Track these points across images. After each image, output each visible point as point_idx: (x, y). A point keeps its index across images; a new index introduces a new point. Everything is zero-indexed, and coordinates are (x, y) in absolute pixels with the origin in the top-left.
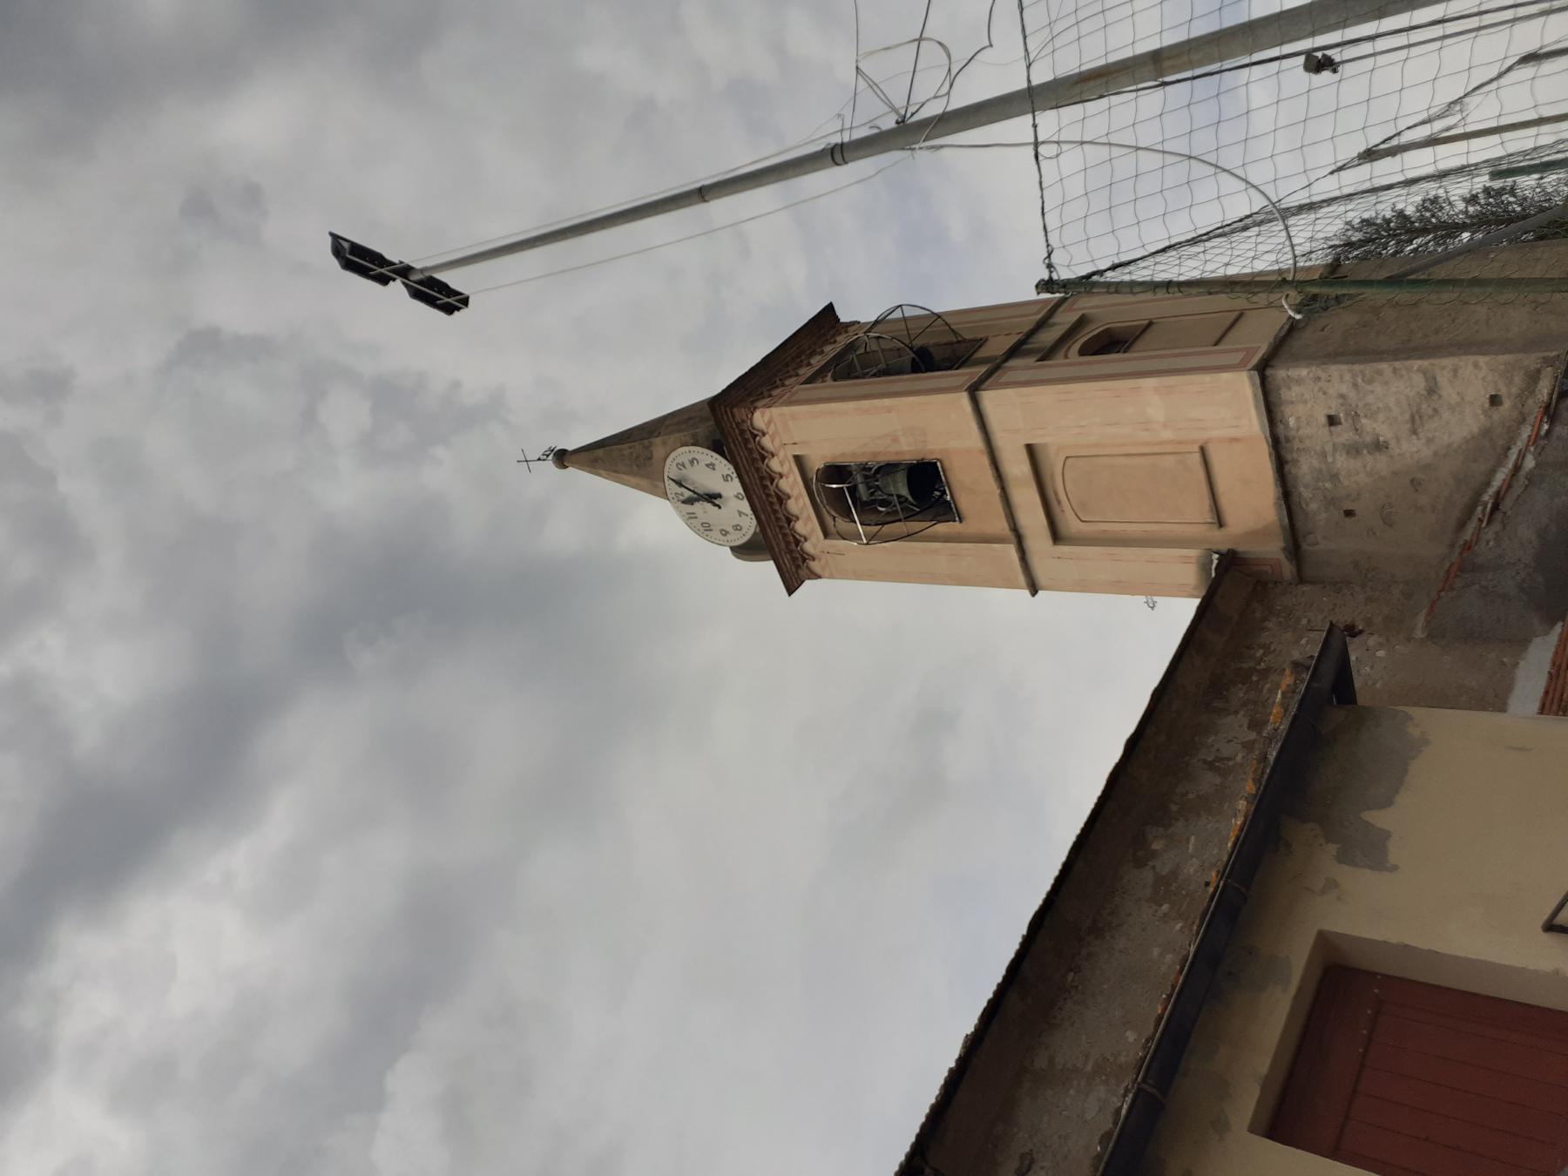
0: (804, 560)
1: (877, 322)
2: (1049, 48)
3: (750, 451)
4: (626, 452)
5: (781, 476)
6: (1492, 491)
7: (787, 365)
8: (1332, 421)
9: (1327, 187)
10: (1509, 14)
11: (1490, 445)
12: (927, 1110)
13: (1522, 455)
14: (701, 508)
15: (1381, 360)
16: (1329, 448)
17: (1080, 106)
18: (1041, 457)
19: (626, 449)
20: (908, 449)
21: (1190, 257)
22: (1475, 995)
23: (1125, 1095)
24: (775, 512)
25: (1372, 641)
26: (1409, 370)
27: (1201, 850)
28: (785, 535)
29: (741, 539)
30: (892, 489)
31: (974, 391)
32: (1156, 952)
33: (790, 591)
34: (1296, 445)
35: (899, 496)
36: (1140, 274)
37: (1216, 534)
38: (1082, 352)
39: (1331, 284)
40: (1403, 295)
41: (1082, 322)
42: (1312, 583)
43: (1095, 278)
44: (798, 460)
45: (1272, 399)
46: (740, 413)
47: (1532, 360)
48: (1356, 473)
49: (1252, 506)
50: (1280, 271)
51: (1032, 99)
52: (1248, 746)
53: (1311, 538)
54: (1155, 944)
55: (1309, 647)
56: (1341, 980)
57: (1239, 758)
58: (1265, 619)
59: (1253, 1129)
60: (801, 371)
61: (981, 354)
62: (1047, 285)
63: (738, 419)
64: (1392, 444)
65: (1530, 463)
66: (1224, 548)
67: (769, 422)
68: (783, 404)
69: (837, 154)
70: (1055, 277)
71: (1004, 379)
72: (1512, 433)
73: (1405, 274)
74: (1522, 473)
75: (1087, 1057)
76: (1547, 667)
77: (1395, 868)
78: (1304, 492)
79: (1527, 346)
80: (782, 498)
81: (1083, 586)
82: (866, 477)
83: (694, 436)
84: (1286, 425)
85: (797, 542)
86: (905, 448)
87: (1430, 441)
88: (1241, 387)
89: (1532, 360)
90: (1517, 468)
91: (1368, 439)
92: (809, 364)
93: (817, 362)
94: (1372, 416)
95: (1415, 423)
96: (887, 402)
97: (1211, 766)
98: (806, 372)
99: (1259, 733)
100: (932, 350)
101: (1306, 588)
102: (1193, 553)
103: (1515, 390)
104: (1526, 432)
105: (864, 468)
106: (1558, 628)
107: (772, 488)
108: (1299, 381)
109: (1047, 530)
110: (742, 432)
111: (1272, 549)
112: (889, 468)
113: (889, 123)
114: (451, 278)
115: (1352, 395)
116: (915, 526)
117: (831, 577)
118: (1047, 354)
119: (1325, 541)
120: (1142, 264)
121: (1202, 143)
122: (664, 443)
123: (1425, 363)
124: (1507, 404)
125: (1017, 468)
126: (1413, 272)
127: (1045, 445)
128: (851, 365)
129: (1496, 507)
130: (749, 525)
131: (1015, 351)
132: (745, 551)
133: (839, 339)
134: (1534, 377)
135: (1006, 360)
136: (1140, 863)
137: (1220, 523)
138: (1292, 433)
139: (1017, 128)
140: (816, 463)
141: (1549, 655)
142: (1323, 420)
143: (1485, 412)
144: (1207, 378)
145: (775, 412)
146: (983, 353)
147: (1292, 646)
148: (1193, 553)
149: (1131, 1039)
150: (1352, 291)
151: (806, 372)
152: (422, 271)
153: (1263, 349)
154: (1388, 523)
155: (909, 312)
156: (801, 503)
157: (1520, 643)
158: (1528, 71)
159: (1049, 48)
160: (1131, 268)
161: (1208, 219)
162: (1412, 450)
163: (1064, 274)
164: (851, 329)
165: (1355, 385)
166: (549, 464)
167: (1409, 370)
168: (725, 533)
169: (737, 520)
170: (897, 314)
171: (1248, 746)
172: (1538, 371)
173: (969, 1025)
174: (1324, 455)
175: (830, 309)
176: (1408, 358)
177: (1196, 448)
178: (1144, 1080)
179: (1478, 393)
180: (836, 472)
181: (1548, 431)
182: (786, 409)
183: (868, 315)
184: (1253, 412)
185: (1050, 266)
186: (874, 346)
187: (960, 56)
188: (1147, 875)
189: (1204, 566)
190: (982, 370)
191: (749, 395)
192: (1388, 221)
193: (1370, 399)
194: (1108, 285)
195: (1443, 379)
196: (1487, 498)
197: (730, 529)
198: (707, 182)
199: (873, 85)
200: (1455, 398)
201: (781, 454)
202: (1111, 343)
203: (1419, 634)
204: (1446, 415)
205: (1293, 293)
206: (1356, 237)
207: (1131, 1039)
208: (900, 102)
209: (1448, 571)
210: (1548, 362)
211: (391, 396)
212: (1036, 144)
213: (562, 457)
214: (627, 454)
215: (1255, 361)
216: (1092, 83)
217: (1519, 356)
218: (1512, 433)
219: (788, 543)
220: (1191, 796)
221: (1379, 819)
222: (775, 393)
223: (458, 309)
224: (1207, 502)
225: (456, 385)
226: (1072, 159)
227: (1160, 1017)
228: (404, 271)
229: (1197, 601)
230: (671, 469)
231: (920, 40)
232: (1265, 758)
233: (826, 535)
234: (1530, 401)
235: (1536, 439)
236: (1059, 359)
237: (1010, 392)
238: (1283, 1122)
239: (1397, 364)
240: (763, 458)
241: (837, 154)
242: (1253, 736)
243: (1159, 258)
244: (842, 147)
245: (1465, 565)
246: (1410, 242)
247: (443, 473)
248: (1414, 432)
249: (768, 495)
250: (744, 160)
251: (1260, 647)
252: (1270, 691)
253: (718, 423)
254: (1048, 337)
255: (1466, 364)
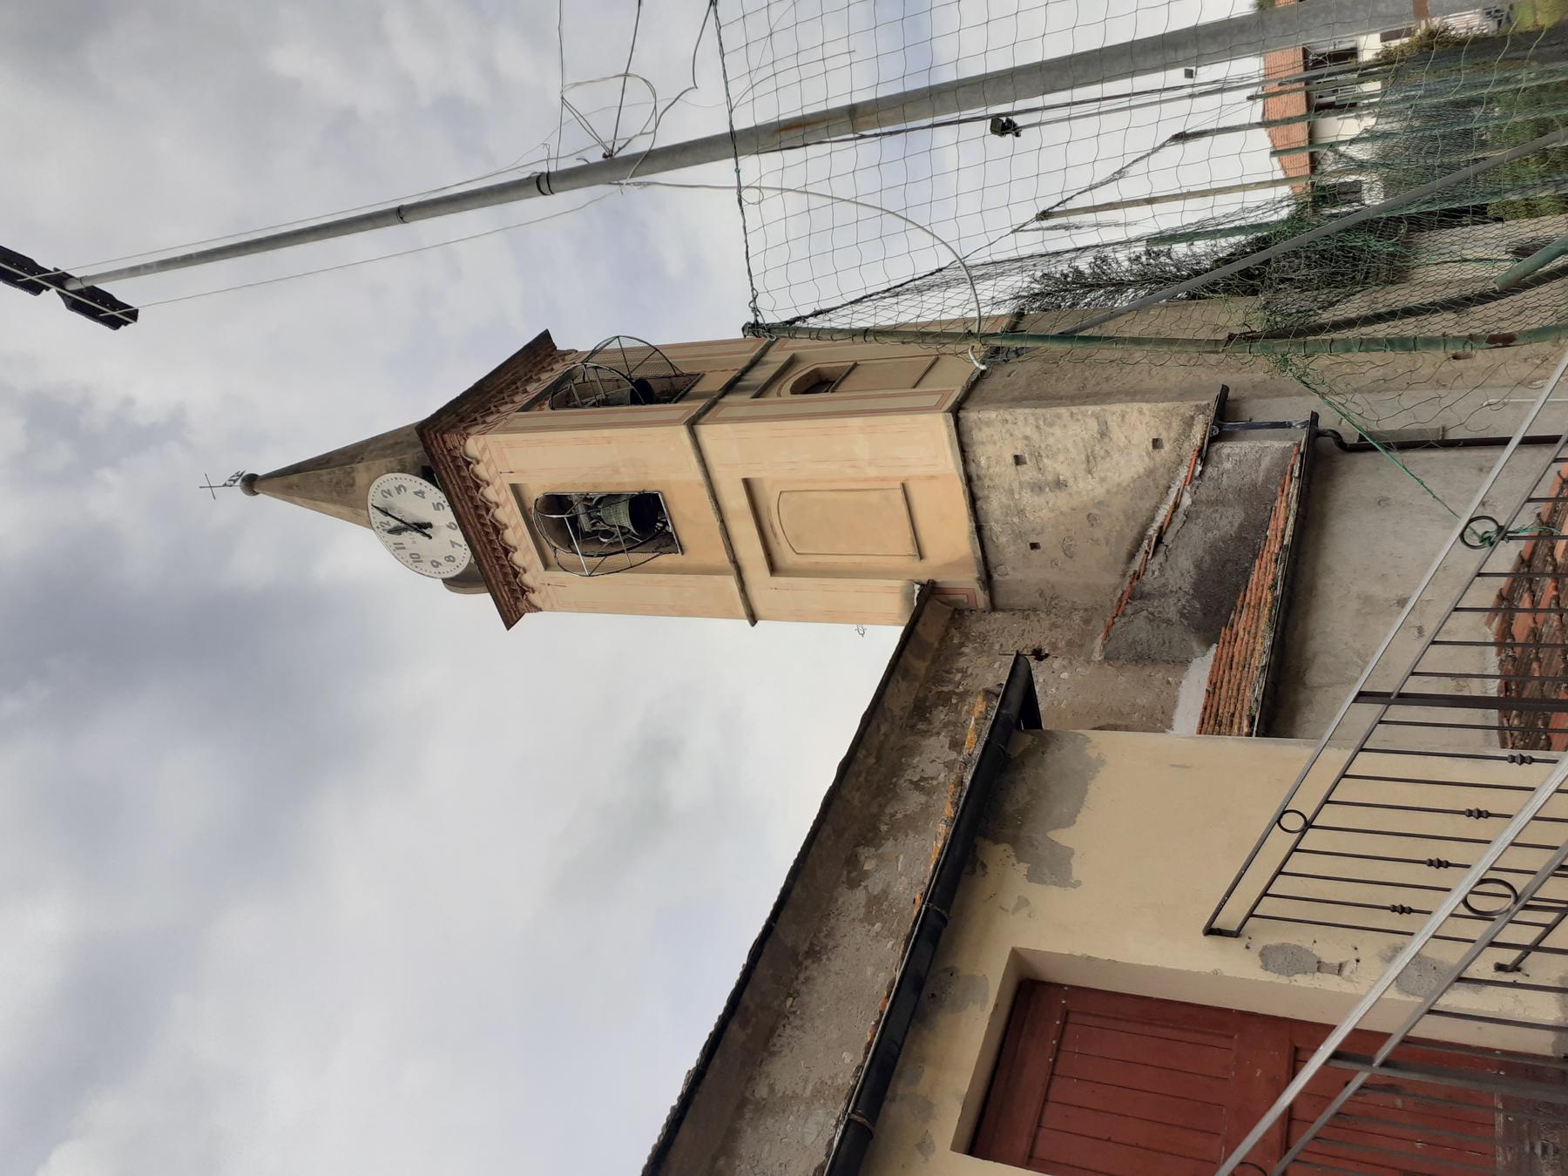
0: (524, 592)
1: (594, 352)
2: (749, 96)
3: (463, 479)
4: (325, 478)
5: (497, 506)
6: (1156, 526)
7: (501, 392)
8: (1018, 460)
9: (1008, 248)
10: (1156, 97)
11: (1154, 483)
12: (649, 1152)
13: (1180, 495)
14: (409, 537)
15: (1059, 405)
16: (1016, 485)
17: (778, 154)
18: (756, 489)
19: (325, 475)
20: (630, 481)
21: (885, 308)
22: (1150, 998)
23: (836, 1127)
24: (491, 542)
25: (1057, 664)
26: (1084, 414)
27: (906, 868)
28: (502, 566)
29: (454, 571)
30: (614, 521)
31: (692, 424)
32: (870, 971)
33: (509, 625)
34: (987, 482)
35: (621, 527)
36: (839, 321)
37: (918, 565)
38: (794, 391)
39: (1012, 338)
40: (1079, 349)
41: (792, 362)
42: (1003, 610)
43: (798, 323)
44: (515, 489)
45: (966, 439)
46: (452, 439)
47: (1186, 408)
48: (1041, 510)
49: (949, 546)
50: (965, 321)
51: (735, 143)
52: (949, 765)
53: (1001, 569)
54: (864, 964)
55: (996, 673)
56: (1032, 994)
57: (941, 778)
58: (962, 645)
59: (954, 1148)
60: (517, 398)
61: (698, 389)
62: (754, 328)
63: (449, 445)
64: (1071, 482)
65: (1187, 501)
66: (924, 579)
67: (484, 449)
68: (497, 431)
69: (543, 183)
70: (760, 320)
71: (722, 414)
72: (1172, 473)
73: (1076, 331)
74: (1181, 510)
75: (806, 1081)
76: (1205, 685)
77: (1078, 883)
78: (994, 527)
79: (1182, 395)
80: (498, 529)
81: (799, 616)
82: (588, 508)
83: (401, 462)
84: (978, 465)
85: (516, 574)
86: (626, 479)
87: (1103, 480)
88: (938, 427)
89: (1186, 408)
90: (1176, 506)
91: (1050, 478)
92: (525, 391)
93: (534, 389)
94: (1054, 456)
95: (1090, 462)
96: (606, 432)
97: (917, 785)
98: (522, 399)
99: (960, 753)
100: (647, 384)
101: (998, 615)
102: (898, 583)
103: (1173, 435)
104: (1183, 472)
105: (586, 498)
106: (1213, 650)
107: (488, 517)
108: (989, 424)
109: (765, 563)
110: (454, 459)
111: (965, 580)
112: (611, 499)
113: (596, 156)
114: (120, 290)
115: (1035, 436)
116: (636, 557)
117: (552, 609)
118: (761, 392)
119: (1015, 572)
120: (841, 312)
121: (893, 201)
122: (368, 469)
123: (1097, 408)
124: (1167, 447)
125: (735, 501)
126: (1082, 329)
127: (761, 480)
128: (569, 394)
129: (1159, 540)
130: (463, 557)
131: (730, 388)
132: (458, 583)
133: (556, 367)
134: (1189, 423)
135: (722, 396)
136: (853, 884)
137: (921, 556)
138: (983, 472)
139: (720, 170)
140: (536, 490)
141: (1207, 674)
142: (1011, 460)
143: (1148, 453)
144: (906, 419)
145: (490, 438)
146: (700, 388)
147: (987, 671)
148: (898, 583)
149: (847, 1060)
150: (1029, 344)
151: (522, 399)
152: (81, 280)
153: (957, 392)
154: (1069, 553)
155: (626, 344)
156: (519, 533)
157: (1182, 663)
158: (1177, 149)
159: (749, 96)
160: (830, 315)
161: (901, 272)
162: (1087, 488)
163: (768, 318)
164: (568, 358)
165: (1038, 427)
166: (237, 491)
167: (1084, 414)
168: (436, 564)
169: (450, 551)
170: (615, 345)
171: (949, 765)
172: (1192, 418)
173: (690, 1059)
174: (1012, 492)
175: (545, 337)
176: (1083, 404)
177: (898, 485)
178: (853, 1111)
179: (1143, 438)
180: (556, 502)
181: (1202, 472)
182: (501, 437)
183: (585, 345)
184: (948, 452)
185: (755, 310)
186: (591, 375)
187: (666, 94)
188: (860, 896)
189: (908, 597)
190: (700, 404)
191: (461, 421)
192: (1066, 276)
193: (1051, 440)
194: (810, 331)
195: (1113, 423)
196: (1152, 532)
197: (442, 560)
198: (406, 202)
199: (580, 118)
200: (1123, 442)
201: (497, 482)
202: (818, 383)
203: (1097, 657)
204: (1116, 456)
205: (978, 345)
206: (1037, 287)
207: (847, 1060)
208: (607, 136)
209: (1120, 600)
210: (1201, 410)
211: (51, 414)
212: (739, 188)
213: (251, 483)
214: (327, 479)
215: (950, 403)
216: (792, 133)
217: (1177, 404)
218: (1172, 473)
219: (505, 575)
220: (899, 816)
221: (1062, 837)
222: (489, 419)
223: (127, 323)
224: (909, 535)
225: (129, 402)
226: (774, 206)
227: (870, 1044)
228: (60, 280)
229: (902, 629)
230: (375, 496)
231: (626, 75)
232: (961, 783)
233: (547, 566)
234: (1186, 445)
235: (1191, 479)
236: (772, 397)
237: (727, 427)
238: (978, 1143)
239: (1074, 409)
240: (478, 487)
241: (543, 183)
242: (953, 755)
243: (857, 307)
244: (548, 176)
245: (1135, 594)
246: (1085, 295)
247: (112, 500)
248: (1090, 472)
249: (483, 525)
250: (454, 181)
251: (958, 671)
252: (968, 712)
253: (427, 449)
254: (761, 375)
255: (1132, 409)
